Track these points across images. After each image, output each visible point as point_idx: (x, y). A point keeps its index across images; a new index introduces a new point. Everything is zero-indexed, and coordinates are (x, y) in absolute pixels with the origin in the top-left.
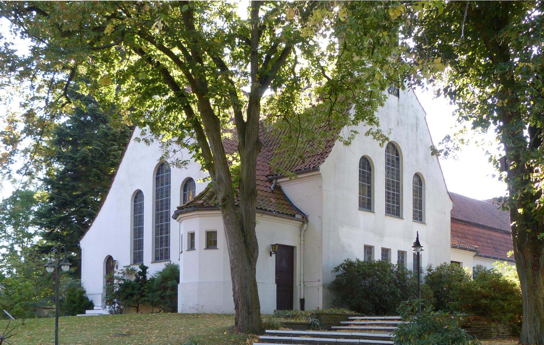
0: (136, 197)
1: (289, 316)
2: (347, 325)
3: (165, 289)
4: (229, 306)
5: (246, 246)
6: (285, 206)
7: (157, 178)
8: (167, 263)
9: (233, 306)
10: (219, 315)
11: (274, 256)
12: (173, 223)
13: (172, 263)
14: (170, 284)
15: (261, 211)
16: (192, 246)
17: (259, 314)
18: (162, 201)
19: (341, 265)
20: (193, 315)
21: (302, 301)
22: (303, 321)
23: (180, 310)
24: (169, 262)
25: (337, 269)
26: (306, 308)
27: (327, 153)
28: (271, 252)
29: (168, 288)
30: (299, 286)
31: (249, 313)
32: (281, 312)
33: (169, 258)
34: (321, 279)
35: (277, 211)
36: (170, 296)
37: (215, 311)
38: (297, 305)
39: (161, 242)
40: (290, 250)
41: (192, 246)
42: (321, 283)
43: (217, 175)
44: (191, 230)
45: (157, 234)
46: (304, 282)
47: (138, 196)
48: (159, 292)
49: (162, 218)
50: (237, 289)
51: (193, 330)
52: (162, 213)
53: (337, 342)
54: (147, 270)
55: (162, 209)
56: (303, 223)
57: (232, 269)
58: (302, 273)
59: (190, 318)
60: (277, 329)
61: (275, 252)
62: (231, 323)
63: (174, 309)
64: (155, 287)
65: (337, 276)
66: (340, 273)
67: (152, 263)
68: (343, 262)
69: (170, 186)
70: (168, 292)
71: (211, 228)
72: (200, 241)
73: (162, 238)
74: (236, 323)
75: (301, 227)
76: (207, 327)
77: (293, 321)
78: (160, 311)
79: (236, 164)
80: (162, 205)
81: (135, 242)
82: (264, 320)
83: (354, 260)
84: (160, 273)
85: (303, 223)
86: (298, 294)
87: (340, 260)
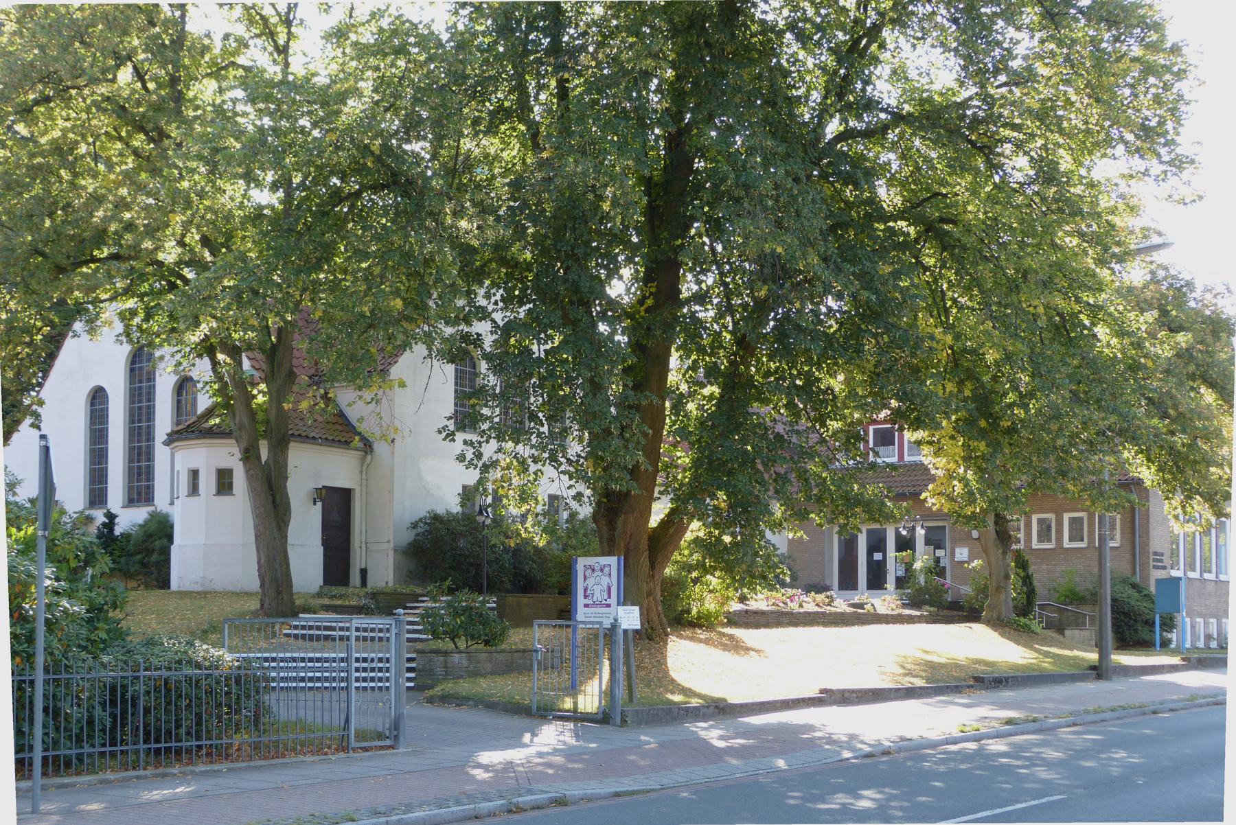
0: (94, 398)
1: (335, 596)
2: (415, 608)
3: (149, 552)
4: (252, 582)
5: (275, 507)
6: (337, 426)
7: (132, 370)
8: (151, 509)
9: (259, 584)
10: (237, 594)
11: (319, 504)
12: (161, 454)
13: (159, 510)
14: (158, 544)
15: (299, 439)
16: (194, 490)
17: (292, 594)
18: (140, 408)
19: (421, 520)
20: (198, 593)
21: (364, 572)
22: (354, 602)
23: (174, 585)
24: (153, 508)
25: (414, 525)
26: (370, 584)
27: (396, 356)
28: (315, 499)
29: (153, 550)
30: (358, 549)
31: (279, 593)
32: (326, 589)
33: (153, 500)
34: (391, 538)
35: (324, 437)
36: (157, 564)
37: (232, 589)
38: (355, 578)
39: (139, 474)
40: (346, 494)
41: (194, 490)
42: (392, 545)
43: (237, 418)
44: (194, 466)
45: (131, 461)
46: (366, 543)
47: (98, 397)
48: (139, 557)
49: (139, 434)
50: (262, 561)
51: (204, 615)
52: (140, 428)
53: (992, 808)
54: (117, 520)
55: (140, 421)
56: (366, 453)
57: (257, 536)
58: (364, 529)
59: (195, 598)
60: (315, 613)
61: (321, 499)
62: (254, 605)
63: (165, 583)
64: (131, 548)
65: (418, 535)
66: (420, 530)
67: (123, 507)
68: (422, 514)
69: (154, 386)
70: (154, 558)
71: (224, 464)
72: (207, 482)
73: (139, 468)
74: (262, 605)
75: (363, 460)
76: (223, 610)
77: (339, 602)
78: (139, 586)
79: (260, 399)
80: (140, 415)
81: (92, 471)
82: (298, 602)
83: (441, 511)
84: (140, 526)
85: (366, 453)
86: (358, 560)
87: (421, 510)
